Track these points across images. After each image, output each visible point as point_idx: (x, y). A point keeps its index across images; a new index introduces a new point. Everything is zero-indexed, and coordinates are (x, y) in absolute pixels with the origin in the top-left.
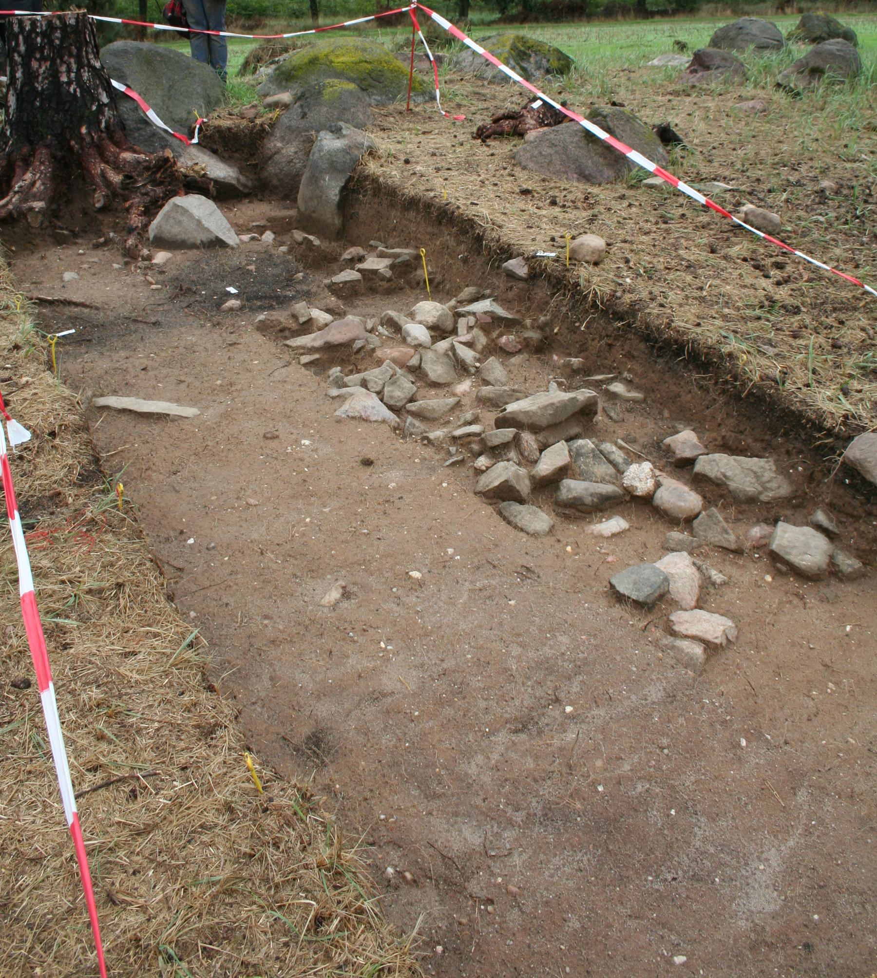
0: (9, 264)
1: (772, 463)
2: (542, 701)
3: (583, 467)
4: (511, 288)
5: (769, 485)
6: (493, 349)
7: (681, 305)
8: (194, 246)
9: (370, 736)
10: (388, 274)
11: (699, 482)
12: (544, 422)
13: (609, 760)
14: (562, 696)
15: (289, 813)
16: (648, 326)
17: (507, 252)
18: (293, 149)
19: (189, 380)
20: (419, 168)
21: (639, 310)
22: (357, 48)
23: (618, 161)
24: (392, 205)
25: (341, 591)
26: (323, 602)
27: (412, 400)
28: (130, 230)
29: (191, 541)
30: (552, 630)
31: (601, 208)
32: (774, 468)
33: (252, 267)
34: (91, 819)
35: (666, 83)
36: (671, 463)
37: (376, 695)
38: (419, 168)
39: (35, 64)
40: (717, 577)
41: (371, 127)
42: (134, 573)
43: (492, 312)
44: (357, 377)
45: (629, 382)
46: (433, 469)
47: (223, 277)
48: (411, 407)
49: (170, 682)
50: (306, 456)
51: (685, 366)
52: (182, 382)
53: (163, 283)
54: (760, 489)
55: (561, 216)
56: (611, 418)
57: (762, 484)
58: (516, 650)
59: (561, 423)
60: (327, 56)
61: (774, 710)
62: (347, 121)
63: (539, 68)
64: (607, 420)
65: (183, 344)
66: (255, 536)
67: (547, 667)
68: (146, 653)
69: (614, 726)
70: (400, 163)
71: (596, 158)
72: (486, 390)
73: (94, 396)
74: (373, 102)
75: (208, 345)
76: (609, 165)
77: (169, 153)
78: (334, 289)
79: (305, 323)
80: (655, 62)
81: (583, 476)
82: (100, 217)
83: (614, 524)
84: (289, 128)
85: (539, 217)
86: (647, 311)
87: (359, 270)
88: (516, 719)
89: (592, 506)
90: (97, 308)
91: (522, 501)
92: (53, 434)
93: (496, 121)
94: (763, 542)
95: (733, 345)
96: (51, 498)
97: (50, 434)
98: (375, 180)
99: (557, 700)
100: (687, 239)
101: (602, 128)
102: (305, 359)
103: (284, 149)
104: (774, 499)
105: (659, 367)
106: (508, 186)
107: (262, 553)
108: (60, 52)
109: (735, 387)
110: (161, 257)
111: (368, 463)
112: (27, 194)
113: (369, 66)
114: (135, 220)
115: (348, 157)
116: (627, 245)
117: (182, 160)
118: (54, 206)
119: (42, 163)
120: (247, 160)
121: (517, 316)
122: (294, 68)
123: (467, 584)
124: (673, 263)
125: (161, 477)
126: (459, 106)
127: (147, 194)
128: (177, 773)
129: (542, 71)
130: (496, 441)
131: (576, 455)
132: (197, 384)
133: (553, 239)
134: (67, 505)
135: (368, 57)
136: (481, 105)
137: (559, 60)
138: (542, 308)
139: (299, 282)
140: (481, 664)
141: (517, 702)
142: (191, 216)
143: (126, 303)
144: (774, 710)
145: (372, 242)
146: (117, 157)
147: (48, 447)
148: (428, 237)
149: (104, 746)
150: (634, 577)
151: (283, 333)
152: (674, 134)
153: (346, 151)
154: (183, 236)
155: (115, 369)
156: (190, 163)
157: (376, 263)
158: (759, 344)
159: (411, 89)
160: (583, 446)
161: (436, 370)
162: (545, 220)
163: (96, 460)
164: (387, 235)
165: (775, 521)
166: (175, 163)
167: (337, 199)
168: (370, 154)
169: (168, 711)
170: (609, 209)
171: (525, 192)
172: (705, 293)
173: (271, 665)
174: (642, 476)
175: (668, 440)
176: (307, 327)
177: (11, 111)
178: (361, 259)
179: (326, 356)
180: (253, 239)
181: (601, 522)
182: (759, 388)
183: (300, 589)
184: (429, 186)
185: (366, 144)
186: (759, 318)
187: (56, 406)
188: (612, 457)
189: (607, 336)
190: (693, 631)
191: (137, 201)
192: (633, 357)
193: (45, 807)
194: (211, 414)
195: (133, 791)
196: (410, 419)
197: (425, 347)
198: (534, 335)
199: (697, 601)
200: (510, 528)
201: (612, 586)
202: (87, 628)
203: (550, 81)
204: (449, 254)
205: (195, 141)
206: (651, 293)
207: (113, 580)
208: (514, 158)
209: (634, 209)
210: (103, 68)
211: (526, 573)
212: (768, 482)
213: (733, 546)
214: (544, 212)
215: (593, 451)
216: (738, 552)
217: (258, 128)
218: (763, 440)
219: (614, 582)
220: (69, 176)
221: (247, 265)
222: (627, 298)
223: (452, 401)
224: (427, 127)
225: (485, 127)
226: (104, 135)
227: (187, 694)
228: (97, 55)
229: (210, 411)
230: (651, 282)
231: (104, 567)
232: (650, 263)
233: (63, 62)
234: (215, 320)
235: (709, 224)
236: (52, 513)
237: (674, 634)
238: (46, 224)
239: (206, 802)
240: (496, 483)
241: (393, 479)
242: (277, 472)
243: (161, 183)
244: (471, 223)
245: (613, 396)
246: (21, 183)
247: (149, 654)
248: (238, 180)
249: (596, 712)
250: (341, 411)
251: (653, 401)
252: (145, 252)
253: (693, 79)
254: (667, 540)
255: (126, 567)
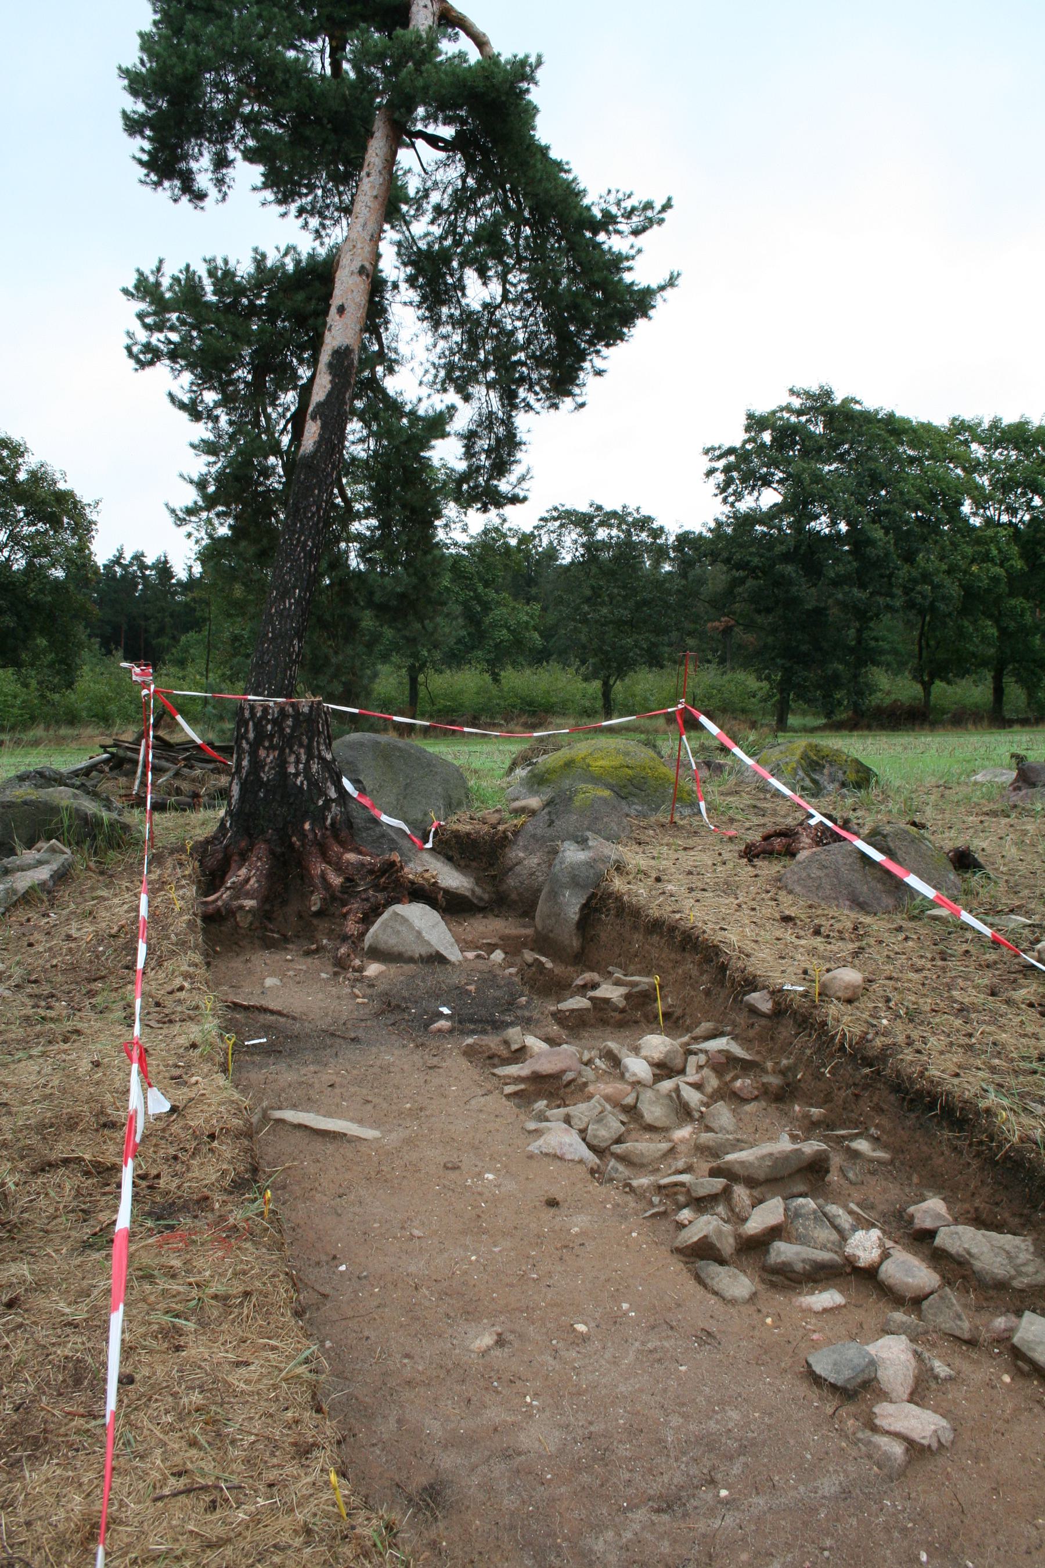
0: (208, 964)
1: (1029, 1243)
2: (695, 1481)
3: (801, 1230)
4: (753, 1024)
5: (1024, 1269)
6: (728, 1094)
7: (942, 1053)
8: (411, 960)
9: (492, 1494)
10: (622, 1004)
11: (938, 1258)
12: (761, 1175)
13: (757, 1554)
14: (719, 1476)
15: (369, 1543)
16: (898, 1074)
17: (751, 984)
18: (536, 861)
19: (376, 1100)
20: (670, 887)
21: (891, 1055)
22: (618, 751)
23: (900, 887)
24: (635, 928)
25: (495, 1337)
26: (472, 1347)
27: (619, 1141)
28: (345, 938)
29: (343, 1268)
30: (722, 1403)
31: (872, 941)
32: (1032, 1249)
33: (472, 988)
34: (165, 1524)
35: (983, 801)
36: (909, 1235)
37: (511, 1452)
38: (670, 887)
39: (262, 753)
40: (941, 1368)
41: (625, 840)
42: (265, 1284)
43: (727, 1051)
44: (562, 1111)
45: (876, 1140)
46: (624, 1217)
47: (438, 995)
48: (617, 1149)
49: (276, 1396)
50: (486, 1191)
51: (939, 1123)
52: (368, 1102)
53: (370, 997)
54: (1013, 1272)
55: (821, 948)
56: (847, 1179)
57: (1016, 1267)
58: (676, 1421)
59: (782, 1178)
60: (584, 759)
61: (984, 1535)
62: (598, 832)
63: (833, 781)
64: (842, 1181)
65: (378, 1063)
66: (412, 1269)
67: (709, 1443)
68: (260, 1367)
69: (769, 1517)
70: (650, 881)
71: (873, 883)
72: (706, 1137)
73: (272, 1108)
74: (633, 812)
75: (406, 1067)
76: (888, 892)
77: (396, 857)
78: (560, 1018)
79: (517, 1051)
80: (979, 778)
81: (802, 1240)
82: (315, 922)
83: (828, 1298)
84: (533, 836)
85: (796, 947)
86: (900, 1057)
87: (591, 999)
88: (661, 1496)
89: (804, 1274)
90: (294, 1018)
91: (722, 1262)
92: (212, 1137)
93: (766, 838)
94: (1006, 1335)
95: (992, 1099)
96: (198, 1202)
97: (209, 1136)
98: (619, 898)
99: (712, 1482)
100: (966, 979)
101: (881, 850)
102: (509, 1089)
103: (525, 860)
104: (1030, 1286)
105: (908, 1123)
106: (767, 912)
107: (416, 1289)
108: (289, 742)
109: (990, 1149)
110: (373, 969)
111: (552, 1203)
112: (239, 891)
113: (630, 772)
114: (351, 927)
115: (592, 871)
116: (892, 982)
117: (411, 865)
118: (267, 907)
119: (259, 859)
120: (485, 870)
121: (757, 1058)
122: (548, 771)
123: (637, 1344)
124: (942, 1005)
125: (325, 1198)
126: (732, 820)
127: (367, 900)
128: (262, 1488)
129: (837, 785)
130: (702, 1192)
131: (792, 1215)
132: (385, 1105)
133: (805, 972)
134: (213, 1210)
135: (631, 762)
136: (756, 820)
137: (858, 772)
138: (785, 1048)
139: (521, 1008)
140: (632, 1432)
141: (666, 1478)
142: (411, 927)
143: (327, 1015)
144: (984, 1535)
145: (610, 969)
146: (340, 858)
147: (205, 1149)
148: (671, 965)
149: (193, 1452)
150: (835, 1356)
151: (493, 1059)
152: (975, 860)
153: (590, 864)
154: (401, 949)
155: (301, 1083)
156: (420, 869)
157: (611, 992)
158: (1023, 1102)
159: (676, 799)
160: (803, 1206)
161: (653, 1111)
162: (801, 950)
163: (255, 1170)
164: (628, 960)
165: (1019, 1314)
166: (402, 868)
167: (576, 917)
168: (618, 869)
169: (268, 1425)
170: (881, 942)
171: (787, 919)
172: (973, 1040)
173: (402, 1407)
174: (868, 1244)
175: (911, 1209)
176: (520, 1054)
177: (233, 801)
178: (595, 986)
179: (532, 1088)
180: (478, 956)
181: (813, 1294)
182: (1018, 1151)
183: (450, 1331)
184: (676, 908)
185: (614, 857)
186: (1035, 1072)
187: (222, 1109)
188: (838, 1221)
189: (854, 1084)
190: (898, 1426)
191: (356, 905)
192: (882, 1110)
193: (121, 1506)
194: (394, 1138)
195: (214, 1502)
196: (613, 1162)
197: (645, 1086)
198: (774, 1081)
199: (912, 1394)
200: (700, 1288)
201: (809, 1365)
202: (204, 1333)
203: (844, 797)
204: (691, 985)
205: (429, 845)
206: (908, 1037)
207: (241, 1289)
208: (780, 880)
209: (910, 943)
210: (334, 760)
211: (706, 1337)
212: (1024, 1265)
213: (966, 1336)
214: (803, 942)
215: (814, 1212)
216: (972, 1343)
217: (500, 834)
218: (1021, 1215)
219: (811, 1360)
220: (287, 874)
221: (467, 984)
222: (879, 1042)
223: (665, 1146)
224: (690, 843)
225: (753, 845)
226: (328, 833)
227: (292, 1410)
228: (329, 746)
229: (394, 1135)
230: (911, 1026)
231: (235, 1274)
232: (914, 1003)
233: (292, 751)
234: (419, 1040)
235: (995, 963)
236: (196, 1217)
237: (875, 1429)
238: (257, 924)
239: (285, 1521)
240: (695, 1239)
241: (578, 1223)
242: (451, 1204)
243: (384, 889)
244: (716, 950)
245: (855, 1154)
246: (234, 879)
247: (262, 1366)
248: (473, 891)
249: (755, 1500)
250: (535, 1146)
251: (902, 1164)
252: (357, 962)
253: (1015, 798)
254: (888, 1322)
255: (258, 1277)
